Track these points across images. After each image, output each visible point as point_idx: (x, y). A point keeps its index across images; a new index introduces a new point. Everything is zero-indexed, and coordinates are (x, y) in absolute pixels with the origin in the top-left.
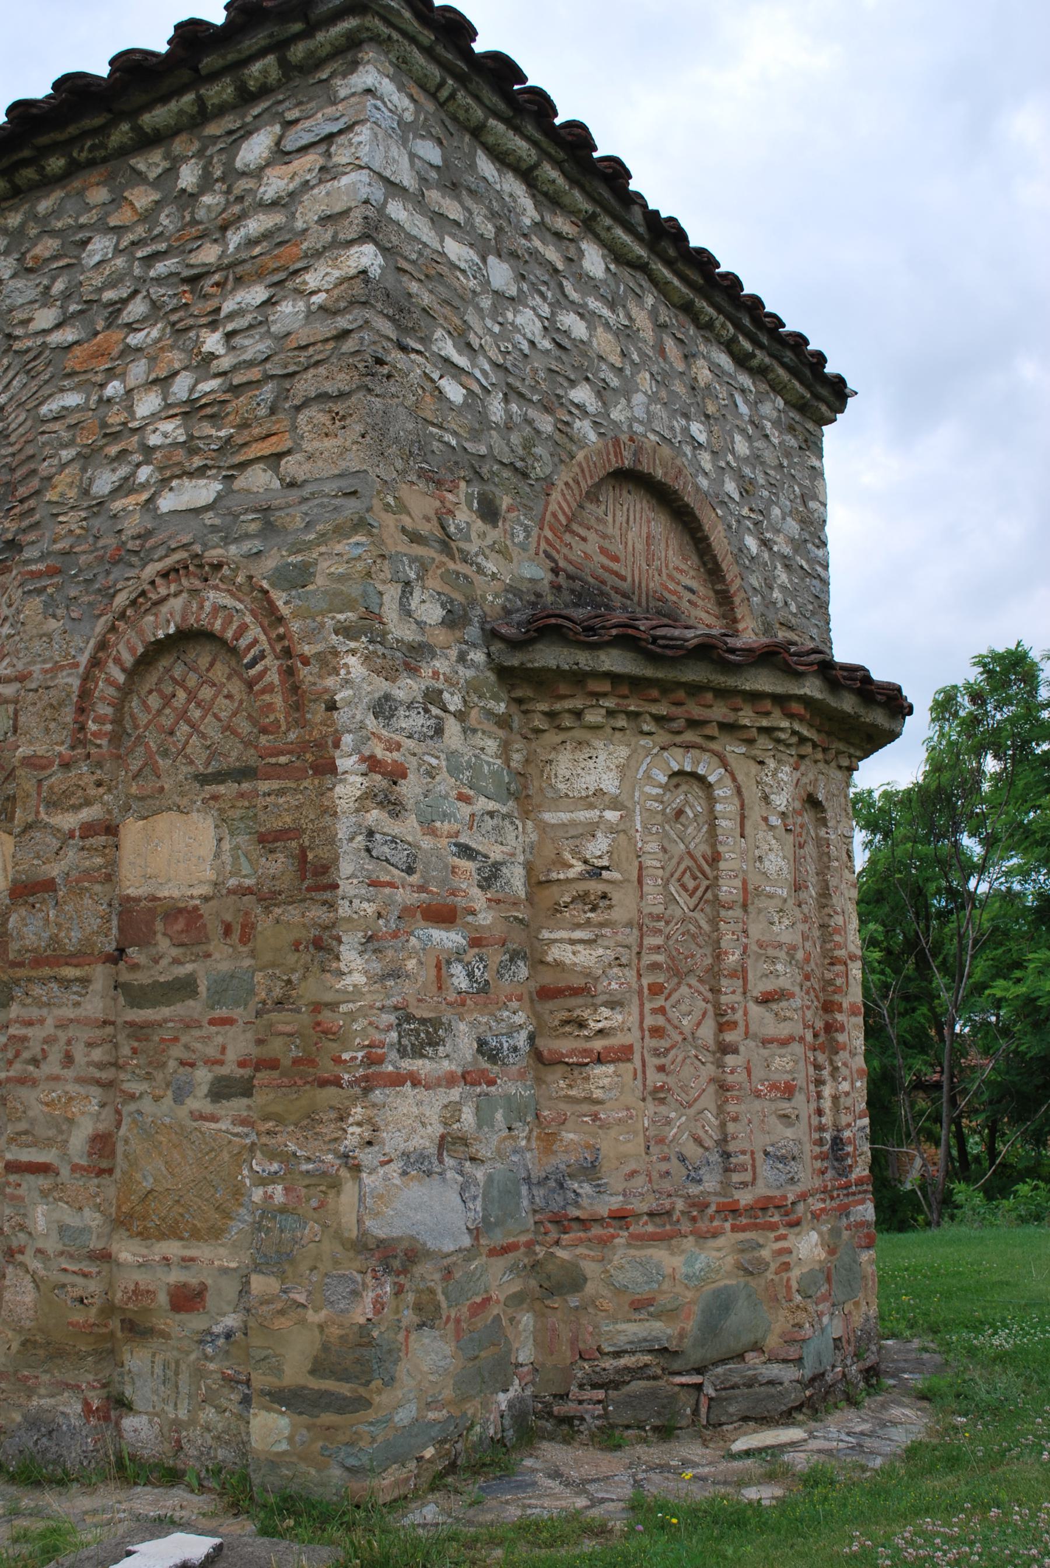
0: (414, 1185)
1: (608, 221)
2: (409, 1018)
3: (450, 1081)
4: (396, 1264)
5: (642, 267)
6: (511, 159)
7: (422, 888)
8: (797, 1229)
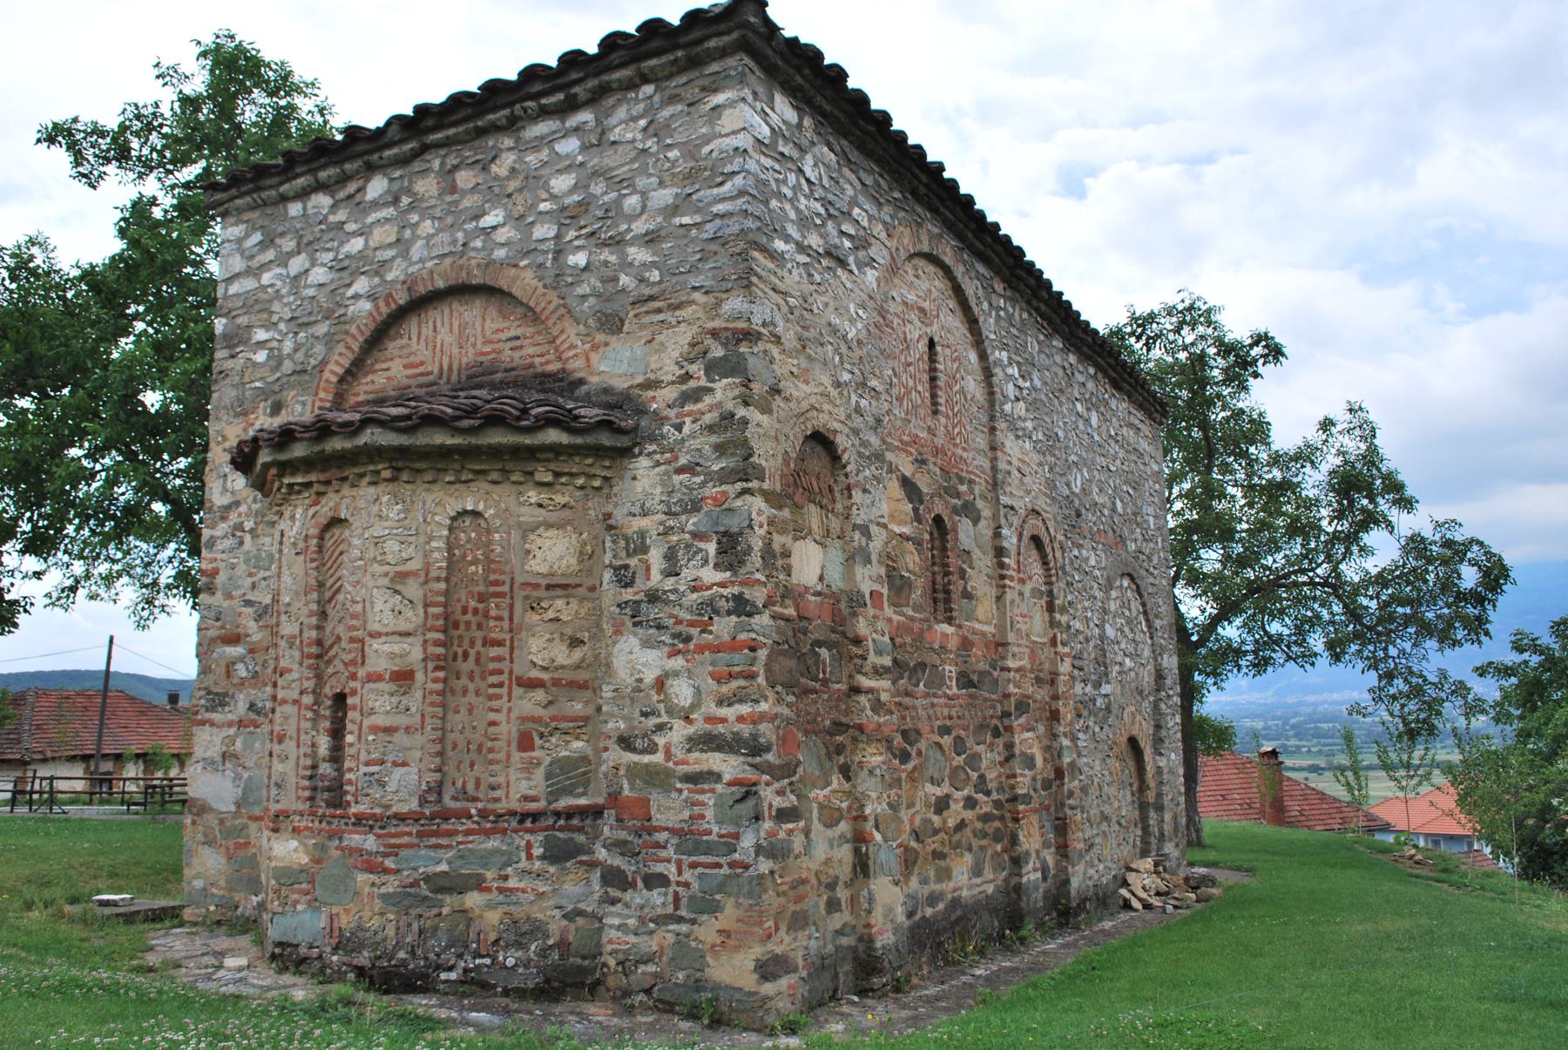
0: (209, 775)
1: (376, 156)
3: (230, 724)
5: (425, 148)
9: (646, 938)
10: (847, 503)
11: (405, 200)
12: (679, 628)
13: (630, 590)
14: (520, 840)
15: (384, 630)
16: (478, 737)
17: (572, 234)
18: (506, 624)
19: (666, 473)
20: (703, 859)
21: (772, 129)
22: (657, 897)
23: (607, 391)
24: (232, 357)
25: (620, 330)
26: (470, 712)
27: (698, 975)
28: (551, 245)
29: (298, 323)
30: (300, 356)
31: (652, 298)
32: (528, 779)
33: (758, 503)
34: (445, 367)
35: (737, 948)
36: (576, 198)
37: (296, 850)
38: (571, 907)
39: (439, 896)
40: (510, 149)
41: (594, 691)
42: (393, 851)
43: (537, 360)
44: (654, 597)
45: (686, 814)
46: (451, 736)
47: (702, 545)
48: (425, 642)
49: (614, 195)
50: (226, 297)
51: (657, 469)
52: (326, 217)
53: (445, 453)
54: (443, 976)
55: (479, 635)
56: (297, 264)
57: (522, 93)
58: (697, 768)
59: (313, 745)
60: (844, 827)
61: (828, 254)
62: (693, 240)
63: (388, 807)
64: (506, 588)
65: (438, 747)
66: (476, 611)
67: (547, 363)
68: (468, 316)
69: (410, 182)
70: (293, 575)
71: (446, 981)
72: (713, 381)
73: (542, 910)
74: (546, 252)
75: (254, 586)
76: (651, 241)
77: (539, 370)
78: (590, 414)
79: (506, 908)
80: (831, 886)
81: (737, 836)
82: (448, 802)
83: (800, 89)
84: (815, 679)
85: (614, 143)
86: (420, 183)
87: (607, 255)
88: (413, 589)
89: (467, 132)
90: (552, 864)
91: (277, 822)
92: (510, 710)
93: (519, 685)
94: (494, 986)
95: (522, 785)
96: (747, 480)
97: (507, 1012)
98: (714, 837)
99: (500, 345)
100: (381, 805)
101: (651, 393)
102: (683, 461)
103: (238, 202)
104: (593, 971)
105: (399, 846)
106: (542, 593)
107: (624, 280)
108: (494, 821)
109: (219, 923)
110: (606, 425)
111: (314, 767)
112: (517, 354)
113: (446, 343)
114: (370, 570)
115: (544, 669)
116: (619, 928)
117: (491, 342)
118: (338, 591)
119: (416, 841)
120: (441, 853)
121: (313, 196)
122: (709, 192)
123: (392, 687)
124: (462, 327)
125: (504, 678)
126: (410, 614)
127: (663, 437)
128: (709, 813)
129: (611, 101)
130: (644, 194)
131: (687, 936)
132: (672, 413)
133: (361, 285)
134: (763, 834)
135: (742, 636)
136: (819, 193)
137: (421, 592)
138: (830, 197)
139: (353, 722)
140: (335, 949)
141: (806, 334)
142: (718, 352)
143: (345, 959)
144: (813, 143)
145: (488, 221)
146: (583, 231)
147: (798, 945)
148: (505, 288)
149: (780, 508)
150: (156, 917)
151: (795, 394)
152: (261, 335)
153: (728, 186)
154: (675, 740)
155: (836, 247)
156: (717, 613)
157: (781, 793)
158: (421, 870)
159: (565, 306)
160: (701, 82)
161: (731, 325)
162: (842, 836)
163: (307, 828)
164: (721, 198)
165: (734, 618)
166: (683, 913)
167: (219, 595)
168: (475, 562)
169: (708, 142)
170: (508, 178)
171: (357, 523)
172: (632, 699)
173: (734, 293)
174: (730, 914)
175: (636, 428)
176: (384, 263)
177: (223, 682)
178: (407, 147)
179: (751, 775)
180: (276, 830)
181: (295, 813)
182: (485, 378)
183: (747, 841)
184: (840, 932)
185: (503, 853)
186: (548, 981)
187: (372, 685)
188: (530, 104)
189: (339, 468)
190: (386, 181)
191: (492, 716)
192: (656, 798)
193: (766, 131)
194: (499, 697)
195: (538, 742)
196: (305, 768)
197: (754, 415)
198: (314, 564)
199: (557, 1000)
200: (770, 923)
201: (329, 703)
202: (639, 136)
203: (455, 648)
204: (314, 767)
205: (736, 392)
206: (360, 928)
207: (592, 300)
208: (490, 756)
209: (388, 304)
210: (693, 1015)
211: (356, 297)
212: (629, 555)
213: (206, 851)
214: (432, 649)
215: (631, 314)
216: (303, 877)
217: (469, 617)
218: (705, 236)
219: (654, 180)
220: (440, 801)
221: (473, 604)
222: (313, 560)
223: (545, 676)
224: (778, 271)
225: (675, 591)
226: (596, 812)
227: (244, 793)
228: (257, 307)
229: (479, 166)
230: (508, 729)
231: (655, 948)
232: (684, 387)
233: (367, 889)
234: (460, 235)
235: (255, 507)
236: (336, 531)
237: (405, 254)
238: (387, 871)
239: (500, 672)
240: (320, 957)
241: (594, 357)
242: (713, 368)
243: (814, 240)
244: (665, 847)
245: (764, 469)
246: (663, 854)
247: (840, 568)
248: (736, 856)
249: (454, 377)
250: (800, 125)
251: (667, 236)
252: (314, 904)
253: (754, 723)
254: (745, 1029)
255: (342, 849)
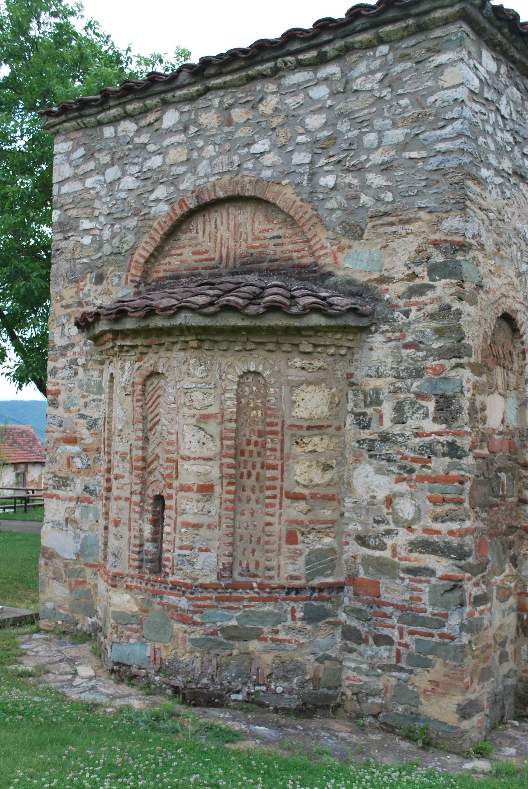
1: (170, 95)
2: (55, 476)
3: (71, 499)
4: (47, 555)
5: (208, 90)
6: (118, 118)
7: (64, 432)
8: (115, 589)
9: (375, 679)
10: (522, 363)
11: (193, 129)
12: (404, 462)
13: (366, 431)
14: (288, 606)
15: (192, 455)
16: (258, 533)
17: (323, 161)
18: (278, 454)
19: (396, 347)
20: (419, 629)
21: (481, 80)
22: (383, 651)
23: (350, 282)
24: (66, 239)
25: (361, 237)
26: (252, 514)
27: (413, 710)
28: (307, 169)
29: (114, 218)
30: (116, 242)
31: (386, 214)
32: (293, 564)
33: (467, 373)
34: (224, 255)
35: (444, 695)
36: (326, 133)
37: (128, 601)
38: (321, 654)
39: (231, 642)
40: (273, 93)
41: (339, 501)
42: (199, 610)
43: (295, 255)
44: (385, 438)
45: (407, 596)
46: (239, 531)
47: (423, 403)
48: (221, 465)
49: (356, 132)
50: (59, 195)
51: (389, 344)
52: (132, 139)
53: (235, 330)
54: (233, 697)
55: (259, 460)
56: (112, 173)
57: (284, 51)
58: (416, 564)
59: (141, 530)
60: (512, 601)
61: (515, 173)
62: (419, 171)
63: (196, 579)
64: (278, 428)
65: (231, 539)
66: (256, 444)
67: (303, 257)
68: (241, 218)
69: (196, 115)
70: (123, 410)
71: (235, 700)
72: (434, 280)
73: (302, 655)
74: (303, 174)
75: (86, 405)
76: (386, 169)
77: (296, 262)
78: (342, 302)
79: (277, 653)
80: (503, 644)
81: (446, 616)
82: (237, 577)
83: (500, 44)
84: (497, 496)
85: (356, 91)
86: (204, 116)
87: (350, 178)
88: (213, 427)
89: (240, 79)
90: (309, 623)
91: (115, 581)
92: (281, 515)
93: (288, 497)
94: (268, 706)
95: (290, 567)
96: (460, 357)
97: (279, 727)
98: (428, 615)
99: (266, 242)
100: (190, 578)
101: (384, 286)
102: (409, 339)
103: (66, 125)
104: (334, 698)
105: (204, 607)
106: (304, 432)
107: (364, 199)
108: (269, 592)
109: (64, 632)
110: (353, 311)
111: (141, 545)
112: (279, 249)
113: (223, 236)
114: (181, 411)
115: (305, 486)
116: (354, 669)
117: (259, 239)
118: (157, 423)
119: (215, 604)
120: (232, 613)
121: (122, 123)
122: (433, 133)
123: (198, 496)
124: (237, 226)
125: (277, 492)
126: (211, 445)
127: (394, 320)
128: (425, 598)
129: (354, 57)
130: (380, 133)
131: (406, 681)
132: (401, 302)
133: (161, 192)
134: (465, 616)
135: (454, 473)
136: (510, 125)
137: (218, 430)
138: (517, 127)
139: (170, 517)
140: (158, 672)
141: (500, 239)
142: (438, 258)
143: (165, 680)
144: (506, 86)
145: (257, 148)
146: (332, 160)
147: (480, 692)
148: (271, 200)
149: (480, 374)
150: (19, 621)
151: (492, 287)
152: (86, 224)
153: (448, 129)
154: (400, 543)
155: (520, 167)
156: (435, 454)
157: (476, 584)
158: (219, 624)
159: (317, 216)
160: (427, 45)
161: (449, 238)
162: (511, 608)
163: (136, 587)
164: (443, 139)
165: (447, 459)
166: (403, 665)
167: (61, 408)
168: (256, 408)
169: (433, 93)
170: (272, 116)
171: (171, 377)
172: (368, 510)
173: (453, 213)
174: (439, 669)
175: (373, 313)
176: (177, 176)
177: (65, 470)
178: (194, 89)
179: (457, 573)
180: (114, 586)
181: (128, 575)
182: (254, 266)
183: (454, 620)
184: (507, 676)
185: (275, 615)
186: (305, 704)
187: (183, 493)
188: (289, 58)
189: (158, 336)
190: (177, 114)
191: (268, 519)
192: (384, 582)
193: (477, 83)
194: (272, 505)
195: (300, 538)
196: (135, 546)
197: (465, 307)
198: (140, 404)
199: (310, 717)
200: (468, 679)
201: (151, 501)
202: (376, 87)
203: (242, 469)
204: (141, 545)
205: (453, 290)
206: (176, 660)
207: (339, 213)
208: (267, 547)
209: (181, 207)
210: (409, 737)
211: (157, 200)
212: (366, 405)
213: (55, 584)
214: (226, 470)
215: (370, 225)
216: (134, 620)
217: (252, 447)
218: (429, 168)
219: (388, 122)
220: (231, 576)
221: (254, 438)
222: (138, 401)
223: (306, 492)
224: (483, 193)
225: (402, 435)
226: (339, 587)
227: (82, 548)
228: (83, 204)
229: (250, 105)
230: (279, 528)
231: (381, 687)
232: (411, 284)
233: (181, 635)
234: (236, 158)
235: (85, 349)
236: (155, 381)
237: (193, 170)
238: (195, 623)
239: (274, 488)
240: (146, 676)
241: (340, 256)
242: (435, 271)
243: (506, 165)
244: (390, 617)
245: (471, 347)
246: (389, 622)
247: (515, 412)
248: (445, 630)
249: (231, 263)
250: (498, 73)
251: (399, 166)
252: (142, 640)
253: (461, 536)
254: (449, 752)
255: (163, 605)
